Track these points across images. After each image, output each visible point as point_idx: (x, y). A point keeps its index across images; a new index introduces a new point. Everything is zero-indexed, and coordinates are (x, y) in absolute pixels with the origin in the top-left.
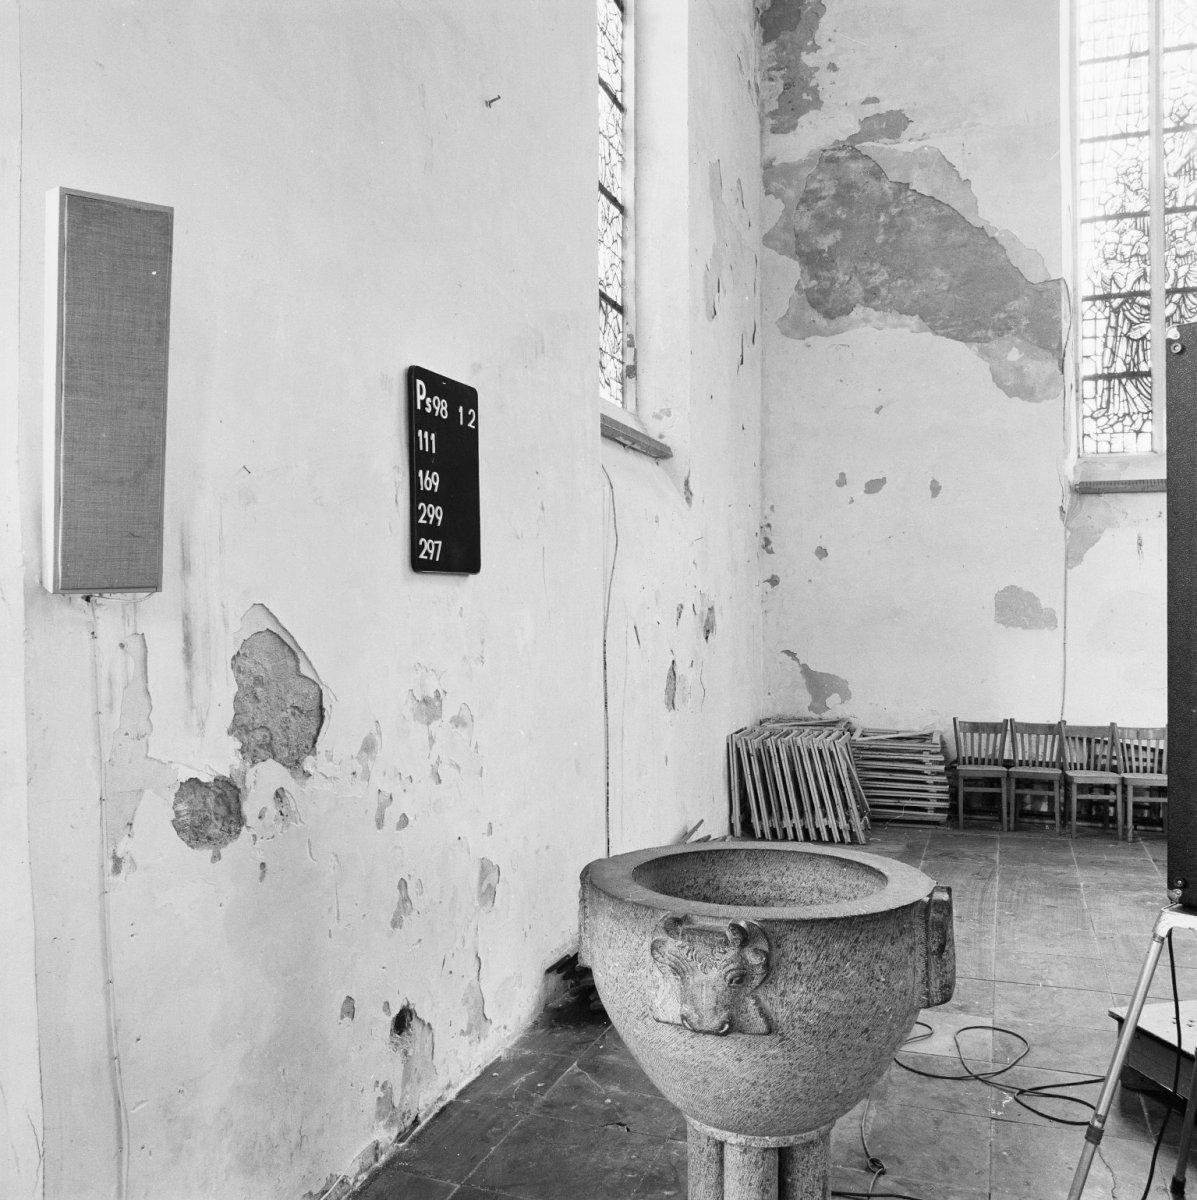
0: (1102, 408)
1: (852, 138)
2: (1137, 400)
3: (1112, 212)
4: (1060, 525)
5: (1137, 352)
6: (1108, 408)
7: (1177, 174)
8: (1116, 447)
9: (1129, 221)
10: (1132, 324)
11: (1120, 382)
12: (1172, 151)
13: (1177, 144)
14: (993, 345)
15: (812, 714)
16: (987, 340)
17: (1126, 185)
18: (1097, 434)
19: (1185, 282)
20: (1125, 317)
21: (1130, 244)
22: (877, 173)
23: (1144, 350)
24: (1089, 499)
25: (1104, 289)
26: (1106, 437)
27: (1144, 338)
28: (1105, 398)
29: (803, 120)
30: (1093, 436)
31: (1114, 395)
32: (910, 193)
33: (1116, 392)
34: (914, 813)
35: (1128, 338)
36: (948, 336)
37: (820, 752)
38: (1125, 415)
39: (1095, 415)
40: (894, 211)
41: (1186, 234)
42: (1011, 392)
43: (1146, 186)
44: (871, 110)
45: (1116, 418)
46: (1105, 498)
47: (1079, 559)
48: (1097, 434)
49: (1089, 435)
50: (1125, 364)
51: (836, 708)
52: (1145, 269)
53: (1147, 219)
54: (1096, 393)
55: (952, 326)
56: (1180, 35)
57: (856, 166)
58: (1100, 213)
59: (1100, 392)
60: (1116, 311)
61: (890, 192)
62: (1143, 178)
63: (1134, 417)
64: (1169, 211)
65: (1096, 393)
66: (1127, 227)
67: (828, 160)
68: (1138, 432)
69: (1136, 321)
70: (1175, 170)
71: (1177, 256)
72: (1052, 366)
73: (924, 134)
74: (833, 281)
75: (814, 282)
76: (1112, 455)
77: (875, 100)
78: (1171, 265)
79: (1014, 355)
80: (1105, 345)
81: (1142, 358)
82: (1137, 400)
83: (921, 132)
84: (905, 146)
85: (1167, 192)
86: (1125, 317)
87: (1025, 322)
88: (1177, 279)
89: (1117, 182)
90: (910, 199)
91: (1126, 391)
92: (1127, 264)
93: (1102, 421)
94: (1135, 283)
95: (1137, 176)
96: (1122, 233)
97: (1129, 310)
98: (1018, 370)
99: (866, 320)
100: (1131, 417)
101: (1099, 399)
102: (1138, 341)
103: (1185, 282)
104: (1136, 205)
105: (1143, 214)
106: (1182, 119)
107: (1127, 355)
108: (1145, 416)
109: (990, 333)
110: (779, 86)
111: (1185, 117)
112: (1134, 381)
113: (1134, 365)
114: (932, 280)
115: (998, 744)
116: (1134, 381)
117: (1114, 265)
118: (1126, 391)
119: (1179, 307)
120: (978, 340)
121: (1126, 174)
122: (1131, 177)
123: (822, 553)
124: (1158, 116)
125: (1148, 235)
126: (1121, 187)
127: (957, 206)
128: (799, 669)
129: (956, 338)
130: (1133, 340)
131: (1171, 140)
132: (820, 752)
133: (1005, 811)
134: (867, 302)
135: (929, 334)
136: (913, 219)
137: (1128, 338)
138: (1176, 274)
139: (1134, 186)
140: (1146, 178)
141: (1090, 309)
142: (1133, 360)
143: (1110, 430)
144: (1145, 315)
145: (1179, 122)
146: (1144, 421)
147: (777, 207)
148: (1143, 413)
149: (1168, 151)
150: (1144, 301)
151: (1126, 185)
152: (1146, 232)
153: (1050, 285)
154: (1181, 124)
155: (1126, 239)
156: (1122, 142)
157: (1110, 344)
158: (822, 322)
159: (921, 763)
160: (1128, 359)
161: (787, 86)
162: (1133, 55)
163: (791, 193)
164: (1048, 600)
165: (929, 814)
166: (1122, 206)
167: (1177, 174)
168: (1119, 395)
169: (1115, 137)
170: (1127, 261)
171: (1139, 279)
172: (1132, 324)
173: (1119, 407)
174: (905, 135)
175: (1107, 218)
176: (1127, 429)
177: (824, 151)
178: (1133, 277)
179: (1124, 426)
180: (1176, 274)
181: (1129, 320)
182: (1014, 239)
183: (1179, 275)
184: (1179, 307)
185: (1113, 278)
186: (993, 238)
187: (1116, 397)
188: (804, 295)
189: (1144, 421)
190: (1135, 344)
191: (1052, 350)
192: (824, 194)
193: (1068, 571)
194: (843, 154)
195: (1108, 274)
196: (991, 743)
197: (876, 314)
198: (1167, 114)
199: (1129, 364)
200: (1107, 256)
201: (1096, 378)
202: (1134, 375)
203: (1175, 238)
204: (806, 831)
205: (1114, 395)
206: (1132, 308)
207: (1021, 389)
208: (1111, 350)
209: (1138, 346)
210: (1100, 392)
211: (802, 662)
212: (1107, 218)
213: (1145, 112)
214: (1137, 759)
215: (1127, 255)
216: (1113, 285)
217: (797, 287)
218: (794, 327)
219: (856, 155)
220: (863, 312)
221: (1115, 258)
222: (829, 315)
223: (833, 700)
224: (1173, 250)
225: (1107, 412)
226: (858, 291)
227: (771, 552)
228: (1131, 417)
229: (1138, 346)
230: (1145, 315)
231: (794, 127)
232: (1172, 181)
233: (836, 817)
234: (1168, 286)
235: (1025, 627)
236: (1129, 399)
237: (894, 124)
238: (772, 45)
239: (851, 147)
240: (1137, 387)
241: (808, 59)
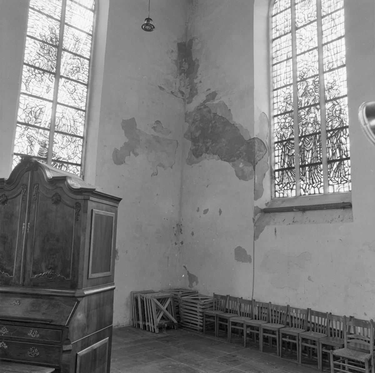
0: (281, 181)
1: (205, 102)
2: (291, 178)
3: (283, 112)
4: (253, 224)
5: (291, 160)
6: (282, 181)
7: (302, 96)
8: (285, 195)
9: (288, 114)
10: (289, 150)
11: (286, 171)
12: (300, 88)
13: (301, 86)
14: (236, 162)
15: (189, 288)
16: (235, 161)
17: (286, 102)
18: (279, 191)
19: (305, 133)
20: (287, 148)
21: (288, 122)
22: (209, 112)
23: (293, 159)
24: (267, 215)
25: (281, 139)
26: (282, 191)
27: (293, 154)
28: (282, 177)
29: (194, 99)
30: (278, 191)
31: (284, 176)
32: (217, 116)
33: (285, 175)
34: (22, 320)
35: (288, 155)
36: (225, 161)
37: (148, 299)
38: (288, 183)
39: (279, 184)
40: (213, 122)
41: (305, 116)
42: (240, 178)
43: (292, 101)
44: (209, 92)
45: (285, 184)
46: (271, 214)
47: (258, 237)
48: (279, 191)
49: (277, 191)
50: (287, 165)
51: (195, 287)
52: (293, 130)
53: (293, 113)
54: (279, 176)
55: (226, 157)
56: (301, 50)
57: (205, 110)
58: (279, 113)
59: (280, 176)
60: (284, 146)
61: (212, 116)
62: (291, 99)
63: (291, 184)
64: (299, 109)
65: (279, 176)
66: (287, 117)
67: (199, 109)
68: (292, 189)
69: (290, 149)
70: (301, 94)
71: (303, 124)
72: (251, 168)
73: (220, 97)
74: (199, 146)
75: (194, 147)
76: (283, 198)
77: (210, 89)
78: (301, 128)
79: (241, 165)
80: (281, 159)
81: (292, 162)
82: (291, 178)
83: (219, 97)
84: (216, 102)
85: (299, 102)
86: (287, 148)
87: (245, 154)
88: (302, 132)
89: (284, 102)
90: (217, 118)
91: (288, 174)
92: (287, 129)
93: (281, 186)
94: (290, 135)
95: (289, 99)
96: (285, 119)
97: (288, 145)
98: (242, 170)
99: (206, 158)
100: (289, 184)
101: (280, 178)
102: (291, 156)
103: (305, 133)
104: (290, 108)
105: (292, 111)
106: (302, 77)
107: (288, 161)
108: (294, 183)
109: (236, 158)
110: (189, 90)
111: (304, 76)
112: (290, 170)
113: (290, 165)
114: (222, 142)
115: (235, 305)
116: (290, 170)
117: (284, 130)
118: (288, 174)
119: (303, 143)
120: (232, 161)
121: (287, 99)
122: (288, 99)
123: (193, 234)
124: (295, 77)
125: (293, 119)
126: (285, 103)
127: (228, 118)
128: (187, 272)
129: (227, 161)
130: (290, 156)
131: (299, 85)
132: (148, 299)
133: (216, 329)
134: (206, 152)
135: (220, 160)
136: (217, 124)
137: (288, 155)
138: (302, 130)
139: (289, 102)
140: (292, 99)
141: (277, 146)
142: (290, 163)
143: (283, 189)
144: (293, 147)
145: (301, 78)
146: (293, 185)
147: (188, 125)
148: (293, 182)
149: (299, 88)
150: (292, 142)
151: (286, 102)
152: (292, 117)
153: (251, 140)
154: (302, 79)
155: (287, 121)
156: (285, 88)
157: (283, 158)
158: (195, 159)
159: (196, 307)
160: (289, 163)
161: (191, 90)
162: (288, 59)
163: (191, 121)
164: (249, 252)
165: (198, 327)
166: (286, 110)
167: (302, 96)
168: (286, 176)
169: (283, 87)
170: (287, 128)
171: (291, 134)
172: (289, 150)
173: (286, 181)
174: (216, 98)
175: (281, 114)
176: (288, 188)
177: (198, 107)
178: (289, 134)
179: (287, 187)
180: (302, 130)
181: (288, 149)
182: (242, 126)
183: (303, 131)
184: (303, 143)
185: (283, 135)
186: (236, 127)
187: (285, 177)
188: (192, 151)
189: (293, 185)
190: (290, 157)
191: (252, 163)
192: (198, 120)
193: (255, 241)
194: (202, 107)
195: (282, 133)
196: (233, 304)
197: (208, 155)
198: (298, 76)
199: (289, 164)
200: (282, 127)
201: (278, 170)
202: (290, 168)
203: (302, 118)
204: (322, 331)
205: (284, 176)
206: (289, 145)
207: (242, 176)
208: (283, 160)
209: (291, 158)
210: (280, 176)
211: (188, 270)
212: (281, 114)
213: (292, 77)
214: (272, 315)
215: (288, 126)
216: (284, 138)
217: (190, 149)
218: (190, 162)
219: (206, 107)
220: (205, 155)
221: (284, 128)
222: (197, 157)
223: (194, 284)
224: (301, 122)
225: (282, 182)
226: (204, 149)
227: (182, 233)
228: (289, 184)
229: (291, 158)
230: (293, 147)
231: (192, 101)
232: (300, 98)
233: (151, 323)
234: (300, 135)
235: (243, 262)
236: (289, 177)
237: (213, 96)
238: (188, 79)
239: (203, 104)
240: (291, 173)
241: (195, 81)
